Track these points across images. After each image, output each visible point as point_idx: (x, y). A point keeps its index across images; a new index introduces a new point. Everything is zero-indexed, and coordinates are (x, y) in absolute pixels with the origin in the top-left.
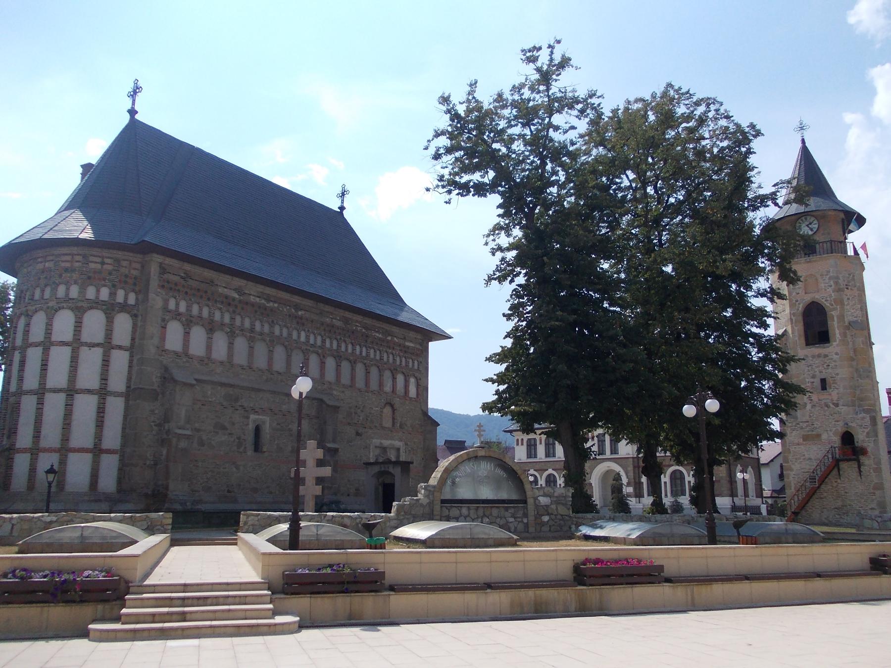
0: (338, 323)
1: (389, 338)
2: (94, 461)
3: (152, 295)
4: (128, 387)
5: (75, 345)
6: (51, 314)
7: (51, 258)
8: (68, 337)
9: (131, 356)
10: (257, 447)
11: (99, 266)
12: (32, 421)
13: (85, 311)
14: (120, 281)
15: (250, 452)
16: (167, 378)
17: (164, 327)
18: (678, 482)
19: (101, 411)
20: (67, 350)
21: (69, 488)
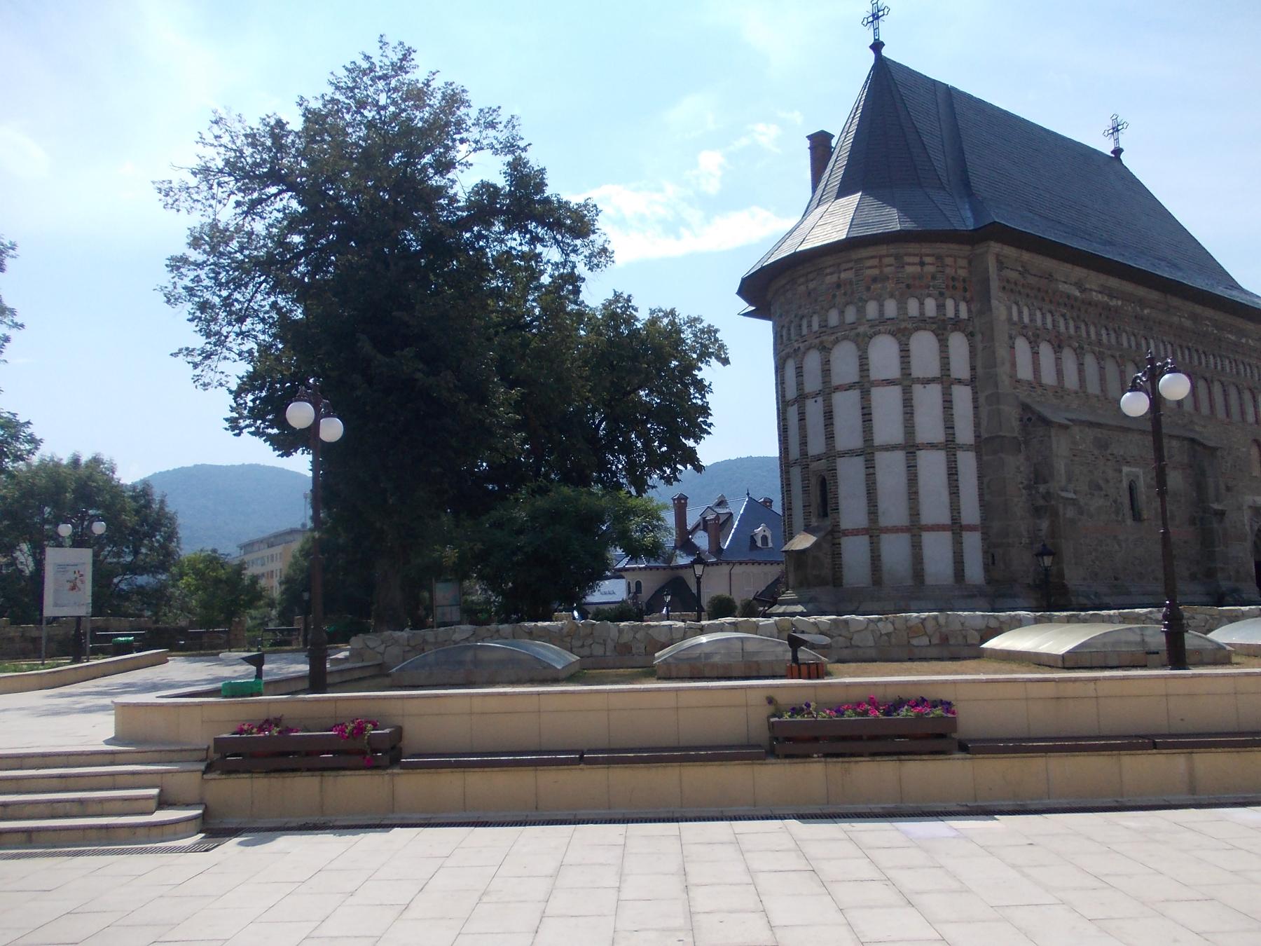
0: (1188, 323)
1: (1244, 340)
3: (994, 303)
4: (977, 436)
5: (906, 383)
6: (862, 345)
8: (894, 372)
9: (975, 393)
11: (918, 269)
14: (947, 287)
15: (1129, 522)
16: (1032, 419)
17: (1013, 347)
19: (952, 472)
20: (855, 395)
21: (929, 580)
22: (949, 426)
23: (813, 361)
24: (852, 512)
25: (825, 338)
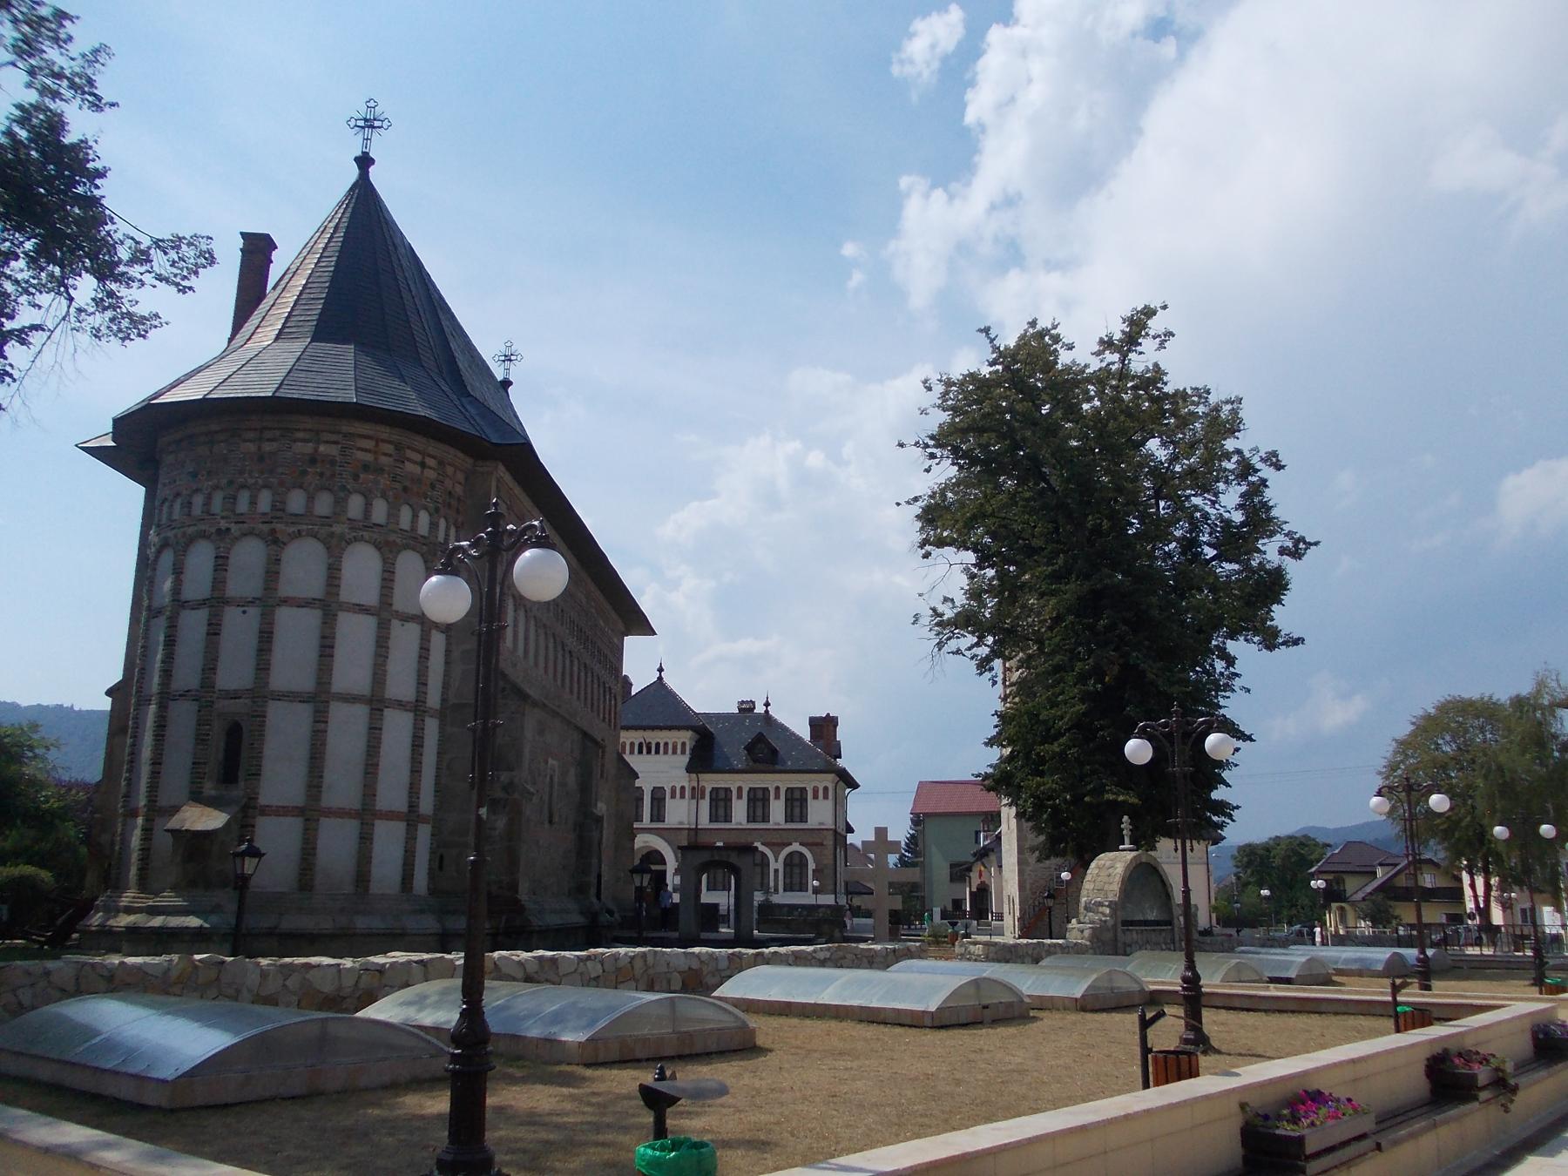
2: (306, 829)
6: (335, 548)
7: (334, 437)
8: (371, 598)
10: (550, 822)
11: (418, 469)
12: (302, 752)
13: (399, 552)
15: (547, 825)
18: (797, 870)
21: (375, 888)
22: (422, 683)
23: (201, 559)
24: (280, 779)
25: (279, 527)
